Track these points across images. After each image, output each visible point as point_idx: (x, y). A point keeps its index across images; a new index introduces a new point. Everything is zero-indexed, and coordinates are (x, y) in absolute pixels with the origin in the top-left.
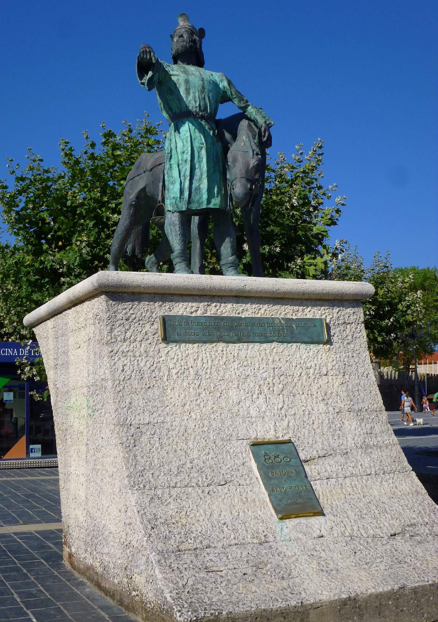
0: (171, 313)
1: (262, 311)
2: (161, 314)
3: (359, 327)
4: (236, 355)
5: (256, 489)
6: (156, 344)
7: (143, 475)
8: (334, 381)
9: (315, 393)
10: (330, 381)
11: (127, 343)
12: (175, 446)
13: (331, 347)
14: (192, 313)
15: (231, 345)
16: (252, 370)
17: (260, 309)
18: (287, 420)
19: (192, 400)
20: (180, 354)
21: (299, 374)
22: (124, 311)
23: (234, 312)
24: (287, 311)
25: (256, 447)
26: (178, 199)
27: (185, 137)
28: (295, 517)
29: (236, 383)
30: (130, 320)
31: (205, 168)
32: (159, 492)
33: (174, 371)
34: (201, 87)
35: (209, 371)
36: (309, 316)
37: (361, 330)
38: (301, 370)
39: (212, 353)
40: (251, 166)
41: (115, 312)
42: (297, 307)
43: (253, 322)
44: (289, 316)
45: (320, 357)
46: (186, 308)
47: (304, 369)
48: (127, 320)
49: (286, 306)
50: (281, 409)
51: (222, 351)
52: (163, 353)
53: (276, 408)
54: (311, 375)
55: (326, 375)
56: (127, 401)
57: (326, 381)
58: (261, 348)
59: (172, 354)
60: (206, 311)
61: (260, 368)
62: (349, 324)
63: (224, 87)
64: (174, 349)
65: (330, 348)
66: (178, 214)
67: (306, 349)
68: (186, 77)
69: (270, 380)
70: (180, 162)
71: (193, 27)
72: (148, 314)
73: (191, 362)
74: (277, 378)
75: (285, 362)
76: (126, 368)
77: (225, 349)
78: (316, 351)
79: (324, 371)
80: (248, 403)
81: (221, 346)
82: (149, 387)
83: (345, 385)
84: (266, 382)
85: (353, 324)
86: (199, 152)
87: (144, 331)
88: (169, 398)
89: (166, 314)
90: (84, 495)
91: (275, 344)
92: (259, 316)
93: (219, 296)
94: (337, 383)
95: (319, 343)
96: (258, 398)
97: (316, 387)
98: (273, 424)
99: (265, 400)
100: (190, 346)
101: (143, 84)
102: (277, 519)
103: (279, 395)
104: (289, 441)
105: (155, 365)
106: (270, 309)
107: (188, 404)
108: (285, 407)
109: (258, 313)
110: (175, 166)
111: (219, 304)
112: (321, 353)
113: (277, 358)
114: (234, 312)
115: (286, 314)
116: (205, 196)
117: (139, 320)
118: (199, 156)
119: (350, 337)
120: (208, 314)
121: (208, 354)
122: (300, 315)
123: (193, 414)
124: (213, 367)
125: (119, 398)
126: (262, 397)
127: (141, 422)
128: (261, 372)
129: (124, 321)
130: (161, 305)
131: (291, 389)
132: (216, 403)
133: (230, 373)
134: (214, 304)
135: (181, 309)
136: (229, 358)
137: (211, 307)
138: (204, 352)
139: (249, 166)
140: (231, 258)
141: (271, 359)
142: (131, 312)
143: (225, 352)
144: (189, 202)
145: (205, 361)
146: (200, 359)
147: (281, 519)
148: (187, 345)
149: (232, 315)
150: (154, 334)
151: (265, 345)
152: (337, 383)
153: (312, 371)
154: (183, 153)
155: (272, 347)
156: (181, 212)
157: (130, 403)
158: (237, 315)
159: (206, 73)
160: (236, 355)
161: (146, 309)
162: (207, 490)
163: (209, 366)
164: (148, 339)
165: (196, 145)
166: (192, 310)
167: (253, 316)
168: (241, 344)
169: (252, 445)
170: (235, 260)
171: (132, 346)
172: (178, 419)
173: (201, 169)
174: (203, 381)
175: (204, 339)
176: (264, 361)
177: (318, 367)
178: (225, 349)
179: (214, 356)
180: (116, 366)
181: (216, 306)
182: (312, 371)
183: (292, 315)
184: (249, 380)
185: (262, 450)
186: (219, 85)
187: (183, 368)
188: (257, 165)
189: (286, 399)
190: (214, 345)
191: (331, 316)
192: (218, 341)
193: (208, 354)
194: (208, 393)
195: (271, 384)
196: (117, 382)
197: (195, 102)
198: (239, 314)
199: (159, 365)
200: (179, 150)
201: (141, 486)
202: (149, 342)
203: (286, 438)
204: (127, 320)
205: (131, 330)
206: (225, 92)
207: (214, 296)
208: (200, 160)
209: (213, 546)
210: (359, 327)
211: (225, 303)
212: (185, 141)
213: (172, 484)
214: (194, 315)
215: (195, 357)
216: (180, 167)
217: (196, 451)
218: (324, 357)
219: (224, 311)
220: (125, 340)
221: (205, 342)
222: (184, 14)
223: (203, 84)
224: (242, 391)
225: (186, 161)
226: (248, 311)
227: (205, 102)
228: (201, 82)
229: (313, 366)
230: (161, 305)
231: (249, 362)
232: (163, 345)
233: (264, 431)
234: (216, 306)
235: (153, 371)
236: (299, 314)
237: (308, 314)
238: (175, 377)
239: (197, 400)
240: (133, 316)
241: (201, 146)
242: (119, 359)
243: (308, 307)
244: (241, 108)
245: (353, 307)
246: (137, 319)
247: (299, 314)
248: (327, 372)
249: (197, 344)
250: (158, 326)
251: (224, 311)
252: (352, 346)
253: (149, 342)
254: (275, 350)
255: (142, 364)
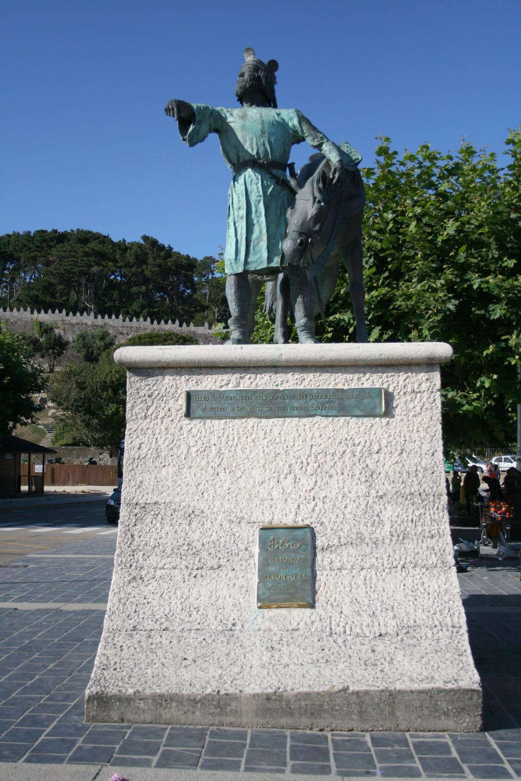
0: (199, 388)
1: (306, 382)
2: (187, 389)
3: (432, 396)
4: (268, 431)
5: (249, 576)
6: (179, 421)
7: (133, 555)
8: (387, 460)
9: (357, 474)
10: (382, 459)
11: (148, 420)
12: (177, 527)
13: (392, 420)
14: (221, 387)
15: (263, 420)
16: (285, 447)
17: (304, 379)
18: (313, 503)
19: (208, 479)
20: (203, 430)
21: (341, 452)
22: (147, 388)
23: (271, 384)
24: (337, 381)
25: (267, 532)
26: (233, 261)
27: (240, 191)
28: (277, 608)
29: (262, 462)
30: (153, 397)
31: (264, 224)
32: (143, 573)
33: (194, 449)
34: (260, 132)
35: (233, 448)
36: (367, 385)
37: (435, 400)
38: (345, 447)
39: (241, 430)
40: (309, 216)
41: (137, 389)
42: (351, 375)
43: (293, 394)
44: (340, 386)
45: (373, 432)
46: (216, 382)
47: (350, 446)
48: (150, 396)
49: (337, 375)
50: (310, 491)
51: (253, 427)
52: (185, 431)
53: (304, 489)
54: (357, 453)
55: (378, 453)
56: (138, 480)
57: (376, 460)
58: (300, 423)
59: (194, 431)
60: (238, 384)
61: (296, 446)
62: (420, 392)
63: (294, 126)
64: (199, 425)
65: (389, 421)
66: (234, 277)
67: (357, 424)
68: (243, 123)
69: (304, 459)
70: (236, 220)
71: (260, 62)
72: (172, 391)
73: (214, 439)
74: (313, 456)
75: (326, 438)
76: (143, 446)
77: (256, 425)
78: (370, 425)
79: (376, 448)
80: (272, 483)
81: (252, 421)
82: (165, 466)
83: (401, 465)
84: (299, 461)
85: (426, 393)
86: (256, 207)
87: (167, 408)
88: (183, 477)
89: (193, 389)
90: (399, 576)
91: (318, 418)
92: (302, 387)
93: (254, 367)
94: (390, 463)
95: (375, 416)
96: (286, 478)
97: (360, 467)
98: (296, 506)
99: (293, 481)
100: (216, 422)
101: (184, 140)
102: (256, 608)
103: (312, 475)
104: (308, 526)
105: (174, 443)
106: (316, 379)
107: (203, 484)
108: (317, 488)
109: (301, 384)
110: (232, 224)
111: (253, 376)
112: (376, 428)
113: (317, 434)
114: (271, 384)
115: (336, 384)
116: (265, 255)
117: (163, 396)
118: (256, 211)
119: (418, 409)
120: (241, 388)
121: (235, 430)
122: (354, 385)
123: (206, 495)
124: (239, 444)
125: (130, 477)
126: (290, 478)
127: (148, 502)
128: (295, 450)
129: (146, 397)
130: (188, 380)
131: (328, 469)
132: (234, 483)
133: (257, 451)
134: (248, 376)
135: (209, 383)
136: (260, 435)
137: (244, 380)
138: (231, 429)
139: (306, 217)
140: (303, 320)
141: (310, 435)
142: (155, 388)
143: (255, 428)
144: (246, 263)
145: (231, 438)
146: (225, 436)
147: (260, 608)
148: (214, 421)
149: (268, 388)
150: (178, 411)
151: (305, 420)
152: (390, 463)
153: (359, 448)
154: (239, 208)
155: (315, 421)
156: (236, 275)
157: (141, 482)
158: (275, 388)
159: (269, 113)
160: (268, 431)
161: (170, 385)
162: (194, 573)
163: (235, 443)
164: (171, 416)
165: (253, 198)
166: (223, 383)
167: (296, 387)
168: (276, 419)
169: (261, 529)
170: (306, 323)
171: (152, 424)
172: (187, 500)
173: (260, 226)
174: (225, 460)
175: (231, 415)
176: (300, 438)
177: (368, 444)
178: (256, 425)
179: (241, 433)
180: (133, 444)
181: (250, 378)
182: (359, 448)
183: (344, 385)
184: (278, 459)
185: (271, 535)
186: (288, 124)
187: (204, 446)
188: (316, 214)
189: (319, 480)
190: (244, 420)
191: (395, 385)
192: (248, 416)
193: (235, 430)
194: (228, 472)
195: (305, 462)
196: (131, 460)
197: (252, 150)
198: (277, 386)
199: (178, 443)
200: (235, 206)
201: (128, 565)
202: (171, 418)
203: (307, 522)
204: (150, 396)
205: (153, 407)
206: (296, 132)
207: (249, 367)
208: (258, 214)
209: (172, 629)
210: (432, 396)
211: (261, 374)
212: (240, 195)
213: (161, 565)
214: (224, 389)
215: (220, 435)
216: (237, 224)
217: (198, 533)
218: (379, 432)
219: (260, 383)
220: (146, 417)
221: (234, 418)
222: (248, 49)
223: (263, 127)
224: (268, 471)
225: (242, 218)
226: (289, 382)
227: (265, 148)
228: (260, 126)
229: (363, 442)
230: (188, 380)
231: (283, 439)
232: (187, 421)
233: (283, 515)
234: (250, 378)
235: (172, 449)
236: (354, 384)
237: (365, 383)
238: (194, 455)
239: (213, 480)
240: (157, 393)
241: (259, 198)
242: (138, 437)
243: (365, 374)
244: (315, 147)
245: (427, 372)
246: (160, 395)
247: (354, 384)
248: (380, 450)
249: (224, 421)
250: (182, 401)
251: (260, 383)
252: (420, 419)
253: (171, 418)
254: (316, 426)
255: (160, 442)
